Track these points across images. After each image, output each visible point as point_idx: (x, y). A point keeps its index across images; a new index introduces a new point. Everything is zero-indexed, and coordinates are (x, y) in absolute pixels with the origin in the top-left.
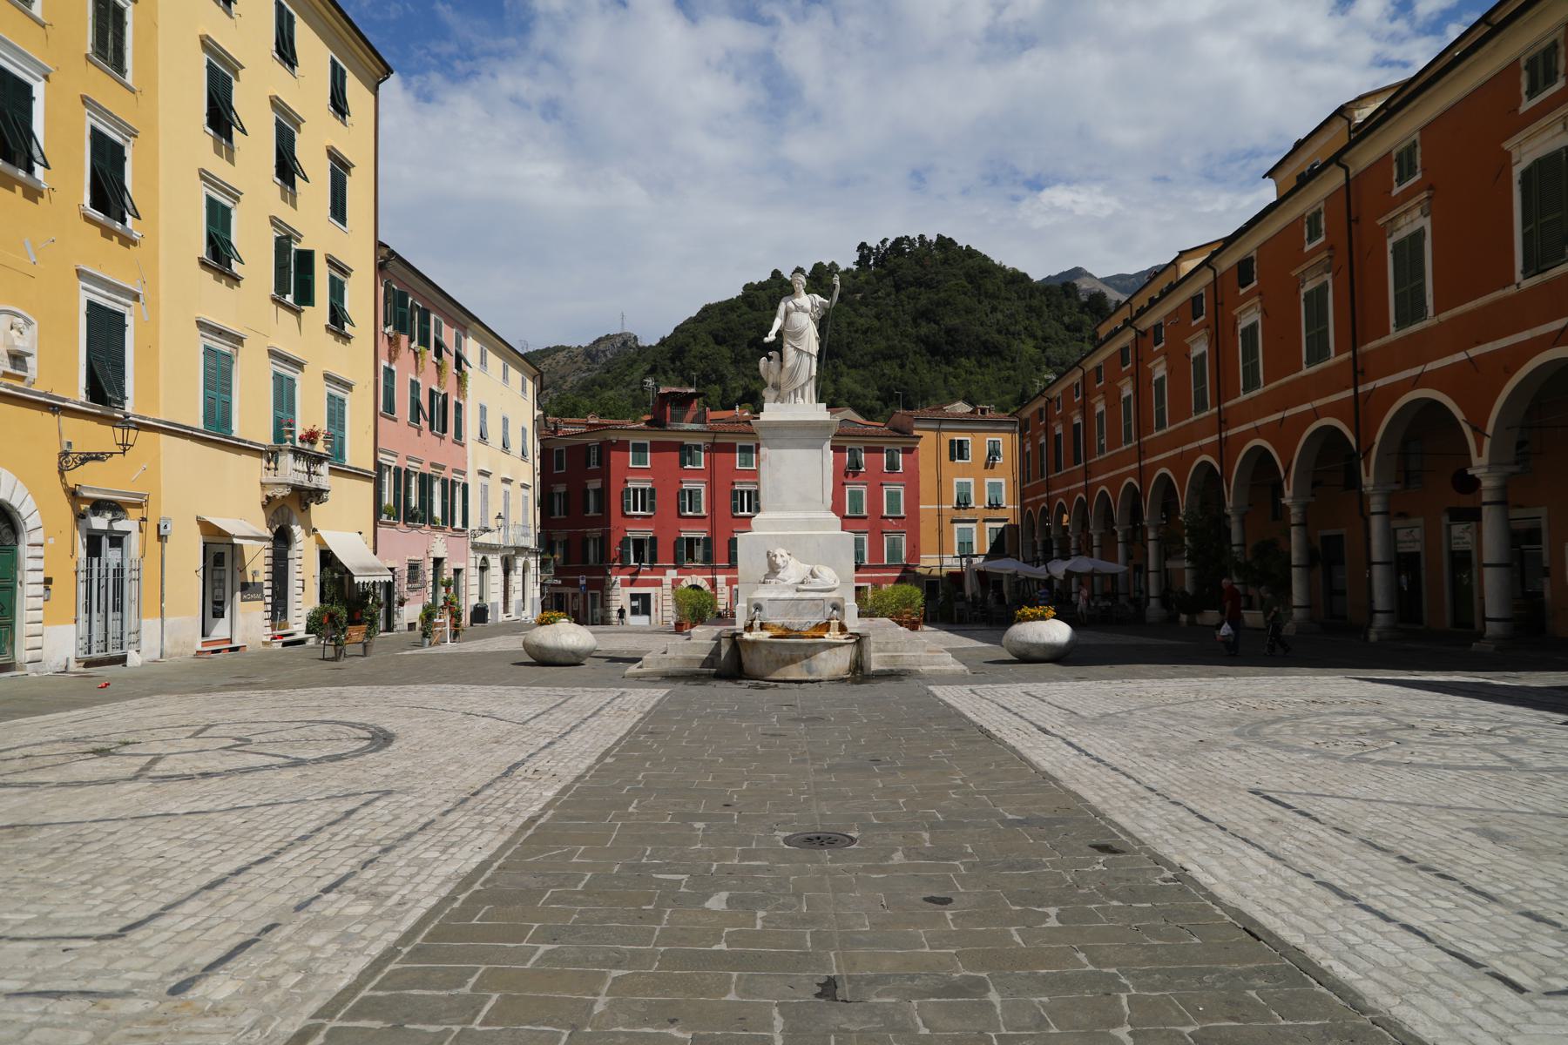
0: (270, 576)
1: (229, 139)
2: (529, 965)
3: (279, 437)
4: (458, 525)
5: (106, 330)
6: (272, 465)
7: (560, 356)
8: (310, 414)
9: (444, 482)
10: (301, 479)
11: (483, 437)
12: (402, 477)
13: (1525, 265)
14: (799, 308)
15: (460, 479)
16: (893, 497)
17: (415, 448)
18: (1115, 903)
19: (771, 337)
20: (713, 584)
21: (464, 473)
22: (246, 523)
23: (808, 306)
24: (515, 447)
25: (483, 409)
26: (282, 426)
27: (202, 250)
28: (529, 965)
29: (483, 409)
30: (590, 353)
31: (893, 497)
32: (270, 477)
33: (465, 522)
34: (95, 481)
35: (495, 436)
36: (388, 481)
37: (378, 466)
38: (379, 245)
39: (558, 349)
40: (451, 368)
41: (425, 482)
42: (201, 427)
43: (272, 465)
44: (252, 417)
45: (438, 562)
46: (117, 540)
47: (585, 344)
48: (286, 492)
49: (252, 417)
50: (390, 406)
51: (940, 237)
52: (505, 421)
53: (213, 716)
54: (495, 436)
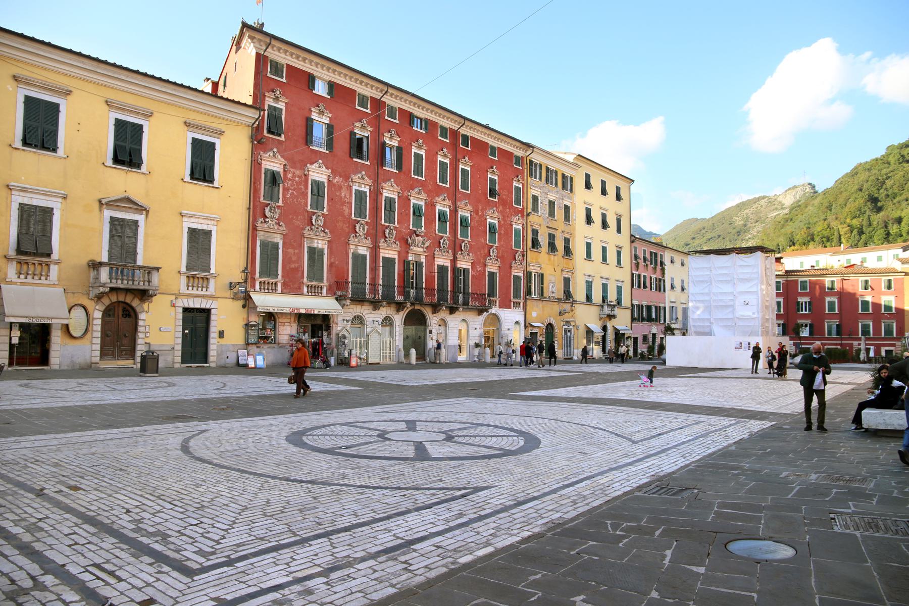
2: (789, 496)
3: (604, 301)
4: (662, 321)
5: (567, 281)
7: (763, 202)
8: (612, 297)
9: (656, 307)
11: (672, 287)
12: (640, 307)
15: (662, 305)
17: (646, 298)
18: (657, 533)
22: (596, 328)
26: (604, 299)
27: (585, 256)
28: (789, 496)
33: (665, 321)
36: (635, 309)
37: (632, 305)
38: (632, 236)
39: (764, 197)
40: (659, 267)
41: (649, 308)
44: (597, 297)
45: (654, 335)
46: (569, 331)
49: (597, 297)
51: (853, 422)
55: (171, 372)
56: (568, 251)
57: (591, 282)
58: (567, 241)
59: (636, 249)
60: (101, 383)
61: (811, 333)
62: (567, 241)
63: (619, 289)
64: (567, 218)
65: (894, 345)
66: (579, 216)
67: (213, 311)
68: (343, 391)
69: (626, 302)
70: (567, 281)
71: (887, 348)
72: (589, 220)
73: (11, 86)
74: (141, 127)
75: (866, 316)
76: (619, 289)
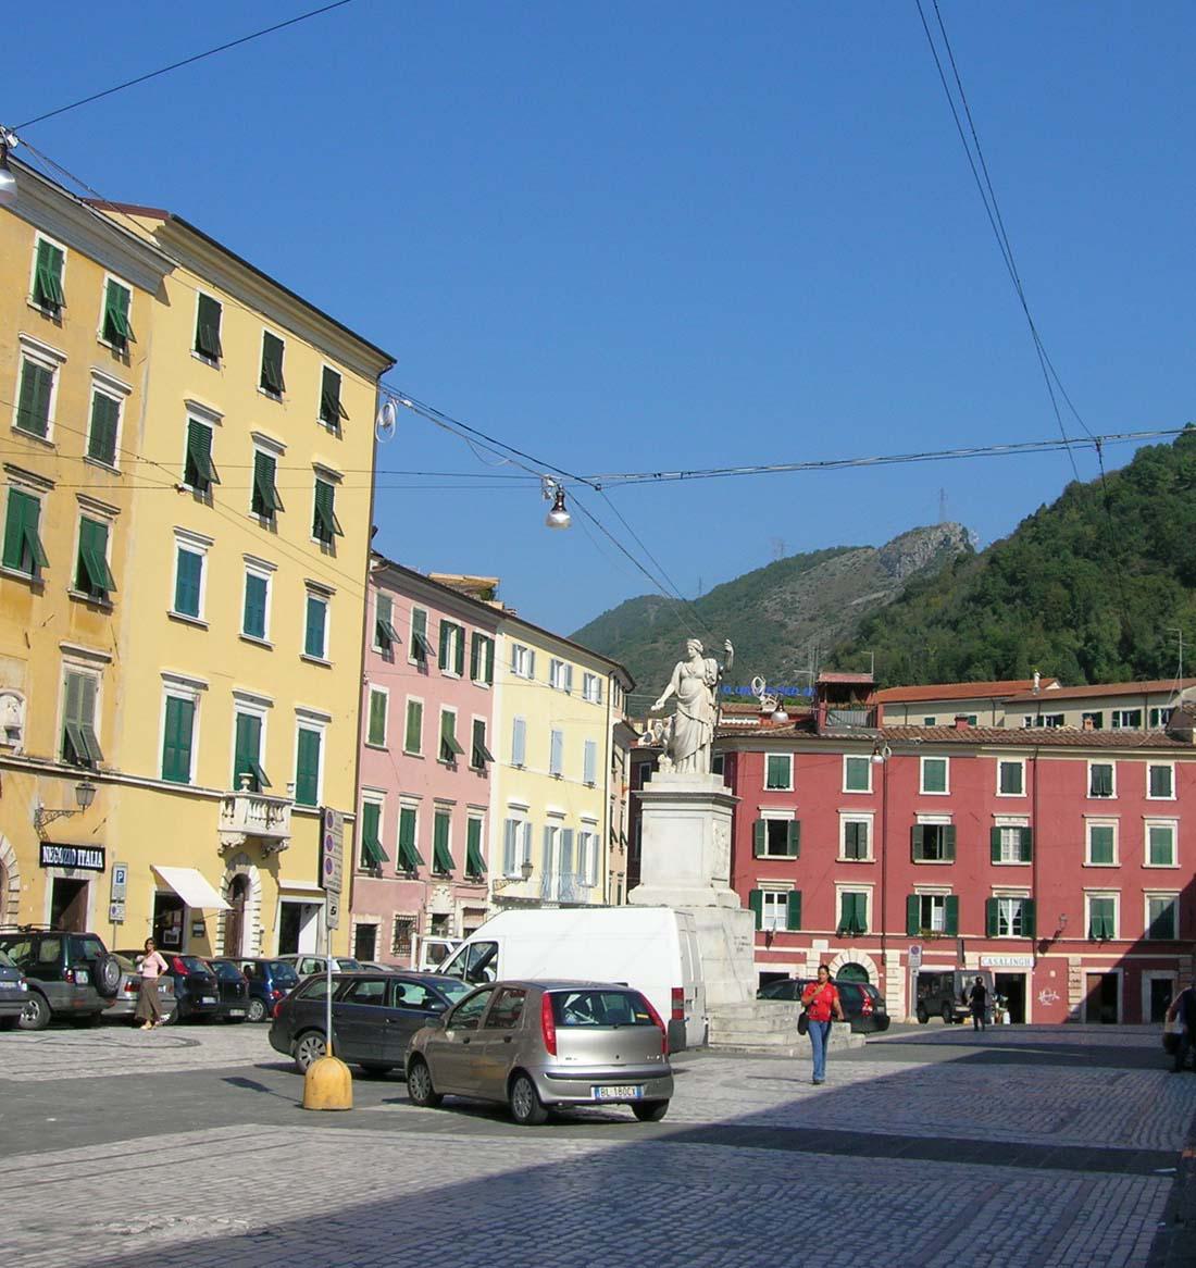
0: (222, 944)
1: (336, 423)
5: (80, 694)
6: (229, 812)
10: (259, 828)
13: (1152, 788)
14: (692, 674)
16: (1161, 837)
19: (659, 705)
20: (881, 962)
21: (485, 809)
23: (701, 671)
24: (574, 772)
25: (519, 726)
29: (519, 726)
30: (887, 560)
31: (1102, 837)
32: (225, 824)
34: (60, 830)
35: (538, 762)
39: (842, 551)
42: (160, 778)
43: (229, 812)
47: (878, 543)
48: (240, 840)
50: (377, 734)
52: (556, 737)
53: (1053, 1136)
54: (538, 762)
55: (1146, 1024)
56: (93, 585)
57: (192, 705)
58: (93, 537)
59: (384, 605)
60: (1017, 1041)
61: (794, 920)
62: (93, 537)
63: (309, 745)
64: (103, 445)
65: (1174, 965)
66: (154, 442)
67: (57, 876)
68: (882, 1082)
69: (333, 792)
70: (80, 694)
71: (1158, 975)
72: (199, 475)
73: (14, 346)
74: (265, 582)
75: (1107, 875)
76: (309, 745)
